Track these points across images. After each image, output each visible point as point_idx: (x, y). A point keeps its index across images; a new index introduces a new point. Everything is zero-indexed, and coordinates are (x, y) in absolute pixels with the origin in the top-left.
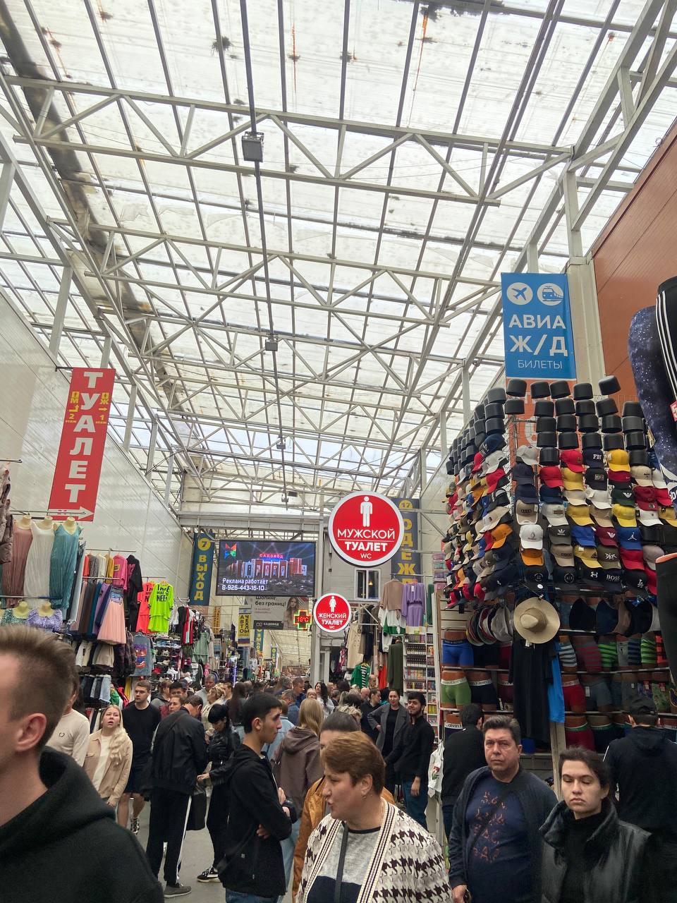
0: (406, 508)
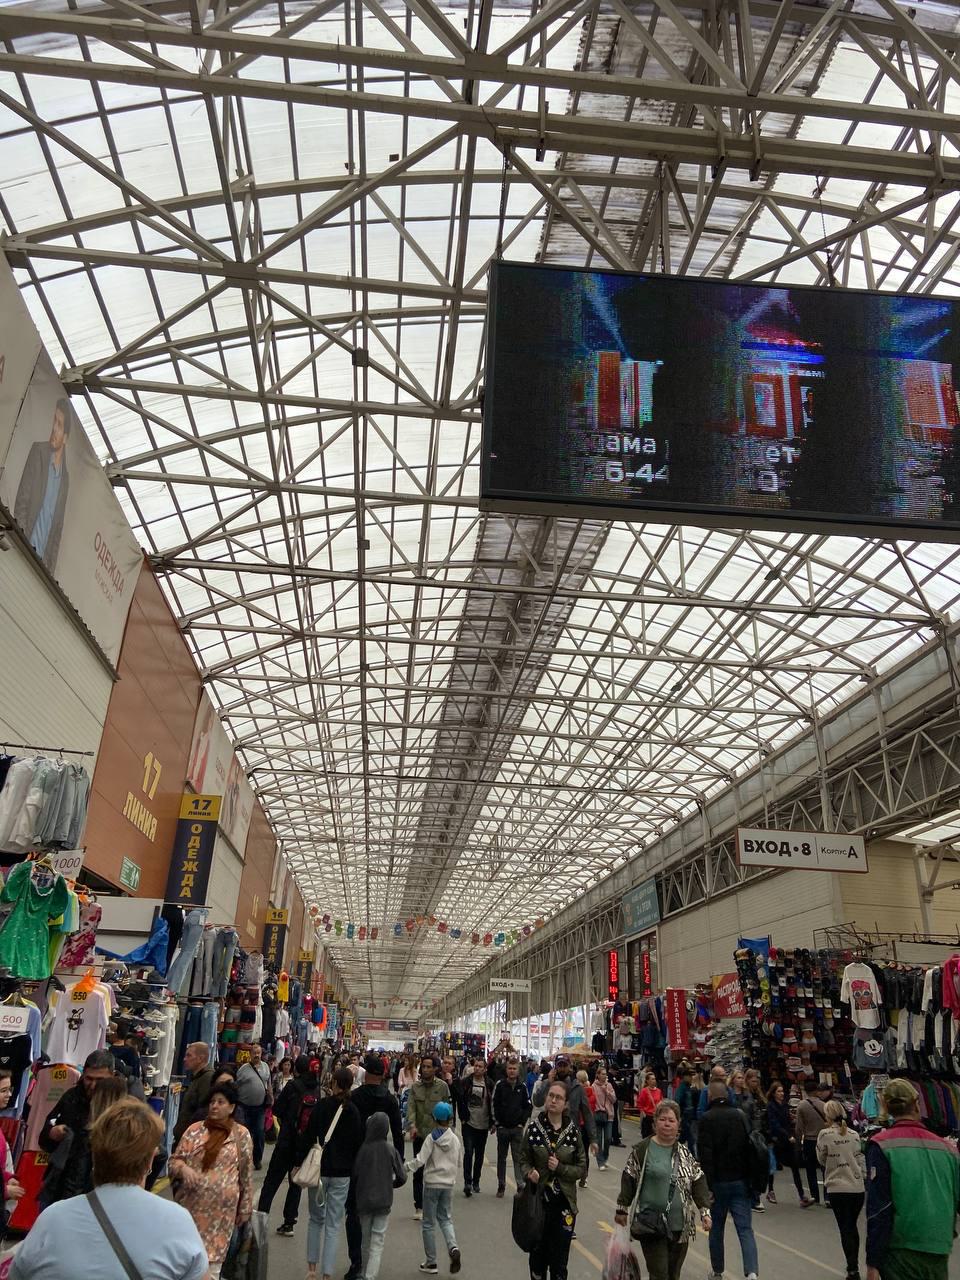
0: (200, 809)
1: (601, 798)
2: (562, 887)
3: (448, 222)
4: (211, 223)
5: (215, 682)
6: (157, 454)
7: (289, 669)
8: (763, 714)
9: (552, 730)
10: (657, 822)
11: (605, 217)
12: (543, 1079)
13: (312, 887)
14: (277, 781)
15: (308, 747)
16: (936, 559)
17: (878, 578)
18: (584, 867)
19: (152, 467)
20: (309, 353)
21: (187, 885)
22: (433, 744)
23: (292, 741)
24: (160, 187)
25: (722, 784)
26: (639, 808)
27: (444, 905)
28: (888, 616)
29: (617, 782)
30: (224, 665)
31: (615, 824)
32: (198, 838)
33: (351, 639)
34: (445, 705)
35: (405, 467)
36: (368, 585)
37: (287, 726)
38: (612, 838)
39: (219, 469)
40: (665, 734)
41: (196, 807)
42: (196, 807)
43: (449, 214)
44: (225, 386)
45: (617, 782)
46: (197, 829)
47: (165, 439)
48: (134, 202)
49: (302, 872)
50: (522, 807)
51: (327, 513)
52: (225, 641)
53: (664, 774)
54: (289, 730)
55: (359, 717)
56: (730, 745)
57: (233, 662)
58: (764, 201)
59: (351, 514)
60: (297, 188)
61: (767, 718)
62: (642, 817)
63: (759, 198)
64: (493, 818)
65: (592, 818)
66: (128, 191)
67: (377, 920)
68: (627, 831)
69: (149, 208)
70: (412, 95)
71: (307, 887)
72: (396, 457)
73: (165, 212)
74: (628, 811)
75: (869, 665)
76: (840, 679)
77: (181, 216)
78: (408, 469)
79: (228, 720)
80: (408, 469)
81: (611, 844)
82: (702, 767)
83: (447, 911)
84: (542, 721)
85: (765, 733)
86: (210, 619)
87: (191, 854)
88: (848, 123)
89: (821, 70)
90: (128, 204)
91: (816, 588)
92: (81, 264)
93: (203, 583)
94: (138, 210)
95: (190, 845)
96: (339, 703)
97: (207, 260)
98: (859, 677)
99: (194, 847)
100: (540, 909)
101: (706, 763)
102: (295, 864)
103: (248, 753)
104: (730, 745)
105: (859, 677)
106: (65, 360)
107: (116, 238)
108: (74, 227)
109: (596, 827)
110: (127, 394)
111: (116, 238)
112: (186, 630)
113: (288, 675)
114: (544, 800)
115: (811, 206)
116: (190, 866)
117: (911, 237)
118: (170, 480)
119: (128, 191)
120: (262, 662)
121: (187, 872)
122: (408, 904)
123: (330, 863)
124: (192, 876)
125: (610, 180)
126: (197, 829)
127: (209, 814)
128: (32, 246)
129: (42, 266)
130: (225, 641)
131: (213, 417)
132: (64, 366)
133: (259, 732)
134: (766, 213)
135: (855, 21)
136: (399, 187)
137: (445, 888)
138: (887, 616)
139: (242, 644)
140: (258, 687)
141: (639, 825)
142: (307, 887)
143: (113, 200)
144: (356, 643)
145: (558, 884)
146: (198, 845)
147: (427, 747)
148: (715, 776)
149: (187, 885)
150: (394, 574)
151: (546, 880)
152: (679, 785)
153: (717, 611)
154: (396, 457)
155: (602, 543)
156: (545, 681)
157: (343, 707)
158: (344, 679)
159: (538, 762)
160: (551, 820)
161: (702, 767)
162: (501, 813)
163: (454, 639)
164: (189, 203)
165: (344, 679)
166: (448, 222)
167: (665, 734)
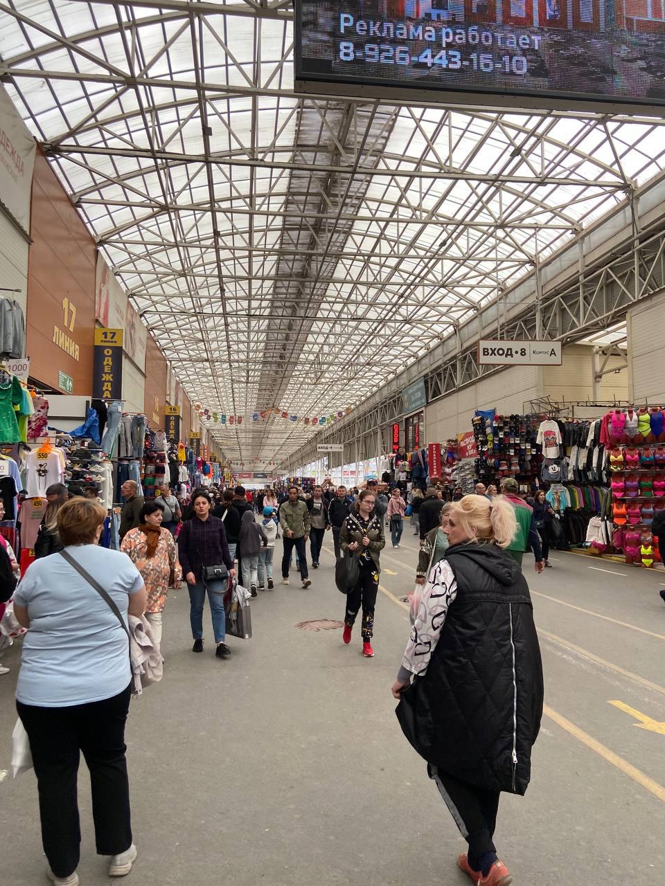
0: (109, 339)
1: (389, 327)
2: (363, 386)
6: (35, 54)
7: (160, 236)
9: (355, 279)
10: (426, 341)
14: (162, 320)
19: (31, 65)
21: (107, 390)
22: (271, 291)
26: (415, 332)
29: (400, 315)
30: (111, 233)
32: (110, 359)
37: (164, 280)
38: (397, 353)
39: (86, 66)
41: (106, 337)
42: (106, 337)
44: (148, 202)
45: (400, 315)
46: (108, 352)
56: (478, 285)
57: (117, 230)
62: (417, 338)
65: (383, 340)
68: (370, 380)
74: (407, 335)
78: (238, 65)
80: (238, 65)
82: (458, 301)
85: (455, 315)
87: (106, 369)
88: (423, 109)
95: (105, 363)
98: (570, 231)
99: (108, 365)
102: (181, 377)
104: (478, 285)
105: (570, 231)
109: (386, 346)
113: (160, 240)
116: (107, 377)
118: (47, 76)
121: (105, 381)
124: (109, 384)
126: (108, 352)
127: (115, 342)
133: (144, 284)
139: (123, 216)
140: (139, 250)
141: (414, 344)
145: (360, 385)
146: (110, 363)
149: (107, 390)
150: (233, 158)
159: (347, 302)
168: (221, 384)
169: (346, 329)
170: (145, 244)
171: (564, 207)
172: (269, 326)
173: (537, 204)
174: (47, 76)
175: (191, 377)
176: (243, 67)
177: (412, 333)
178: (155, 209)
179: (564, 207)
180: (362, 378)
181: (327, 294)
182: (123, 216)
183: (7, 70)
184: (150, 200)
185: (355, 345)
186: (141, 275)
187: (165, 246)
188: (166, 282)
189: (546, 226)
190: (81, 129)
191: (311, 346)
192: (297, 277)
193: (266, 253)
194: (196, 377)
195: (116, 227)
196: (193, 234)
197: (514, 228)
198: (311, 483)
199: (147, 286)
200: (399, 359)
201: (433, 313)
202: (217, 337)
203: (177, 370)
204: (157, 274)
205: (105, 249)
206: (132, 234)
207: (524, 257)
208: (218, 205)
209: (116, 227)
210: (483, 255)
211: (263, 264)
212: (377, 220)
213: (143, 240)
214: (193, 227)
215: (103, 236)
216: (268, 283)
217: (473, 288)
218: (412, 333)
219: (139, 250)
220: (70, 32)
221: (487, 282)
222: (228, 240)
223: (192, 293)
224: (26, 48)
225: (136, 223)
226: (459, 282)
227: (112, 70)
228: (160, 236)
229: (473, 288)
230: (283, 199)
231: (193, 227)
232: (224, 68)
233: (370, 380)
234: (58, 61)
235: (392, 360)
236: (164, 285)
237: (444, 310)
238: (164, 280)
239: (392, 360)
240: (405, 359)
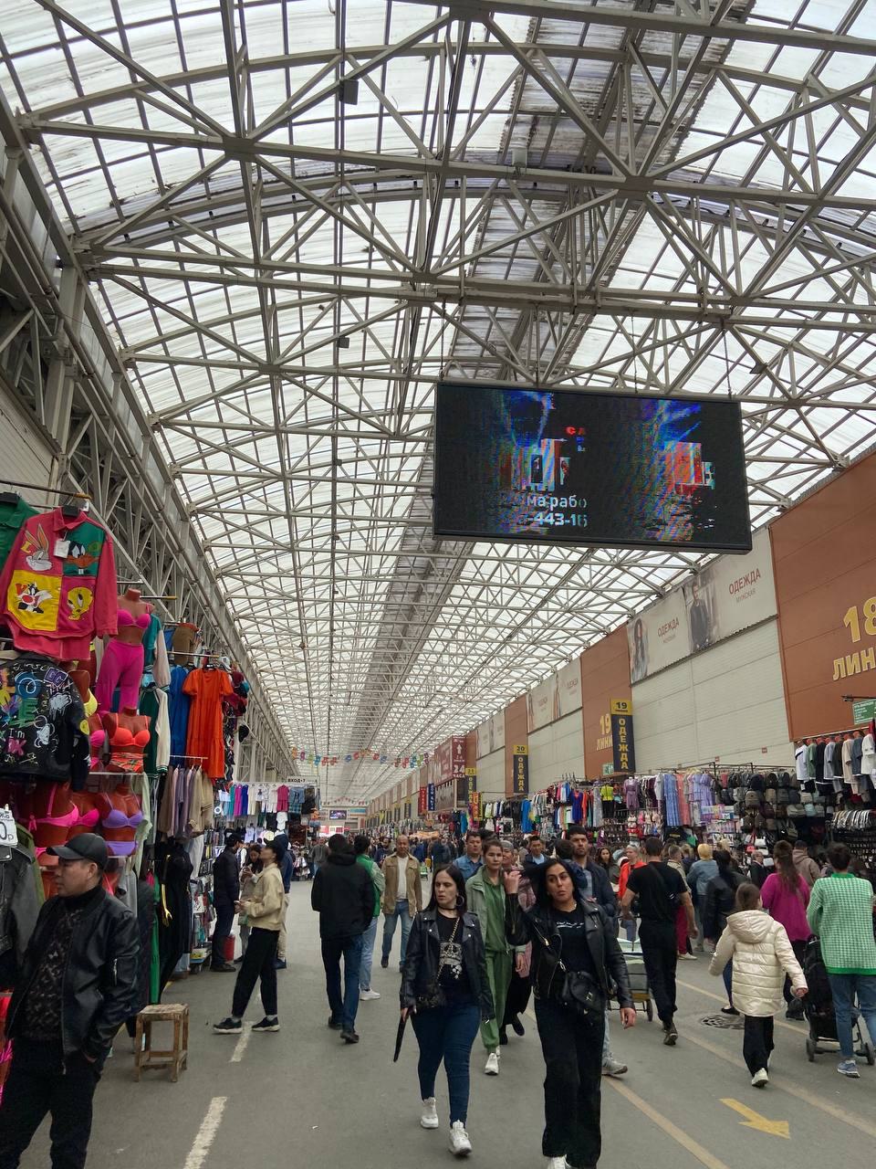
1: (511, 647)
2: (498, 696)
3: (421, 117)
4: (214, 100)
5: (105, 282)
6: (163, 339)
7: (248, 414)
8: (626, 592)
9: (502, 555)
10: (554, 663)
11: (497, 316)
12: (151, 780)
13: (282, 704)
14: (251, 607)
15: (281, 574)
16: (824, 427)
17: (790, 427)
18: (518, 680)
19: (157, 350)
20: (285, 99)
22: (392, 571)
23: (267, 568)
24: (162, 65)
25: (564, 663)
26: (540, 652)
27: (395, 710)
28: (796, 460)
29: (539, 619)
30: (175, 411)
31: (520, 666)
33: (322, 434)
34: (397, 562)
35: (392, 113)
36: (341, 379)
37: (264, 555)
38: (518, 675)
39: (217, 352)
40: (581, 582)
43: (421, 108)
44: (257, 470)
45: (539, 619)
47: (171, 324)
48: (139, 79)
49: (279, 704)
50: (450, 654)
51: (300, 304)
52: (211, 483)
53: (599, 593)
54: (265, 560)
55: (328, 572)
56: (605, 611)
57: (187, 407)
58: (717, 74)
59: (327, 468)
60: (287, 62)
61: (629, 595)
62: (542, 659)
63: (713, 71)
64: (433, 652)
65: (503, 661)
66: (134, 69)
67: (335, 749)
68: (529, 670)
69: (153, 84)
70: (371, 286)
71: (282, 716)
72: (384, 103)
73: (165, 86)
74: (531, 655)
75: (843, 455)
76: (675, 571)
77: (181, 91)
78: (399, 117)
79: (160, 431)
80: (399, 117)
81: (518, 680)
82: (804, 451)
83: (396, 720)
84: (478, 572)
85: (630, 603)
86: (197, 465)
88: (775, 46)
89: (697, 109)
90: (134, 81)
91: (593, 574)
92: (167, 365)
93: (193, 436)
94: (142, 87)
95: (621, 733)
96: (298, 348)
97: (204, 134)
98: (776, 508)
100: (476, 717)
101: (644, 578)
102: (259, 664)
103: (228, 580)
104: (605, 611)
105: (776, 508)
106: (20, 105)
107: (121, 114)
108: (84, 103)
109: (507, 668)
110: (188, 429)
111: (121, 114)
112: (33, 136)
113: (246, 420)
114: (468, 649)
115: (761, 79)
117: (848, 108)
118: (173, 363)
119: (134, 69)
120: (217, 404)
122: (388, 619)
123: (298, 681)
125: (577, 53)
128: (43, 123)
129: (143, 368)
130: (211, 483)
131: (210, 302)
132: (18, 109)
133: (237, 561)
134: (719, 83)
135: (725, 70)
136: (410, 201)
137: (430, 625)
138: (796, 460)
139: (195, 383)
140: (216, 437)
141: (569, 641)
142: (282, 716)
143: (121, 77)
144: (328, 440)
145: (495, 694)
147: (387, 575)
148: (594, 631)
150: (366, 368)
151: (469, 705)
152: (612, 602)
153: (501, 629)
154: (384, 103)
155: (701, 103)
156: (433, 632)
157: (312, 539)
158: (315, 511)
159: (486, 585)
160: (471, 663)
161: (804, 451)
162: (433, 658)
163: (414, 480)
164: (188, 78)
165: (315, 511)
166: (421, 117)
167: (581, 582)
168: (316, 707)
169: (455, 659)
170: (246, 514)
171: (766, 481)
172: (380, 632)
173: (849, 372)
174: (173, 363)
175: (284, 699)
176: (407, 118)
177: (535, 654)
178: (247, 373)
179: (766, 481)
180: (497, 686)
181: (474, 552)
182: (195, 383)
183: (132, 355)
184: (260, 468)
185: (480, 655)
186: (177, 368)
187: (256, 431)
188: (247, 493)
189: (865, 405)
190: (146, 220)
191: (492, 554)
192: (428, 552)
193: (392, 522)
194: (285, 683)
195: (183, 401)
196: (306, 503)
197: (814, 406)
198: (315, 832)
199: (219, 498)
200: (546, 662)
201: (601, 599)
202: (317, 657)
203: (263, 674)
204: (254, 549)
205: (101, 289)
206: (206, 413)
207: (822, 456)
208: (343, 425)
209: (183, 401)
210: (755, 453)
211: (381, 564)
212: (442, 640)
213: (221, 420)
214: (306, 496)
215: (161, 415)
216: (422, 445)
217: (656, 568)
218: (535, 654)
219: (216, 437)
220: (203, 318)
221: (615, 607)
222: (349, 468)
223: (296, 573)
224: (73, 95)
225: (216, 397)
226: (636, 561)
227: (240, 352)
228: (248, 414)
229: (656, 568)
230: (506, 117)
231: (306, 496)
232: (377, 119)
233: (529, 670)
234: (187, 347)
235: (537, 664)
236: (246, 497)
237: (615, 596)
238: (264, 555)
239: (537, 664)
240: (554, 663)
